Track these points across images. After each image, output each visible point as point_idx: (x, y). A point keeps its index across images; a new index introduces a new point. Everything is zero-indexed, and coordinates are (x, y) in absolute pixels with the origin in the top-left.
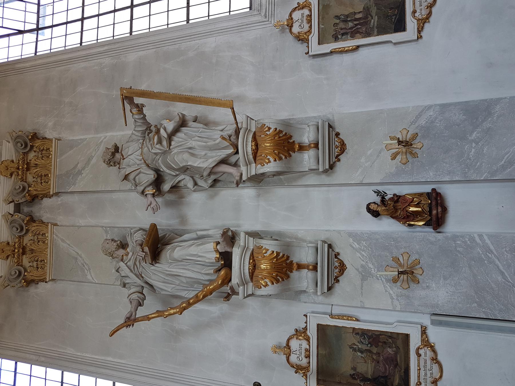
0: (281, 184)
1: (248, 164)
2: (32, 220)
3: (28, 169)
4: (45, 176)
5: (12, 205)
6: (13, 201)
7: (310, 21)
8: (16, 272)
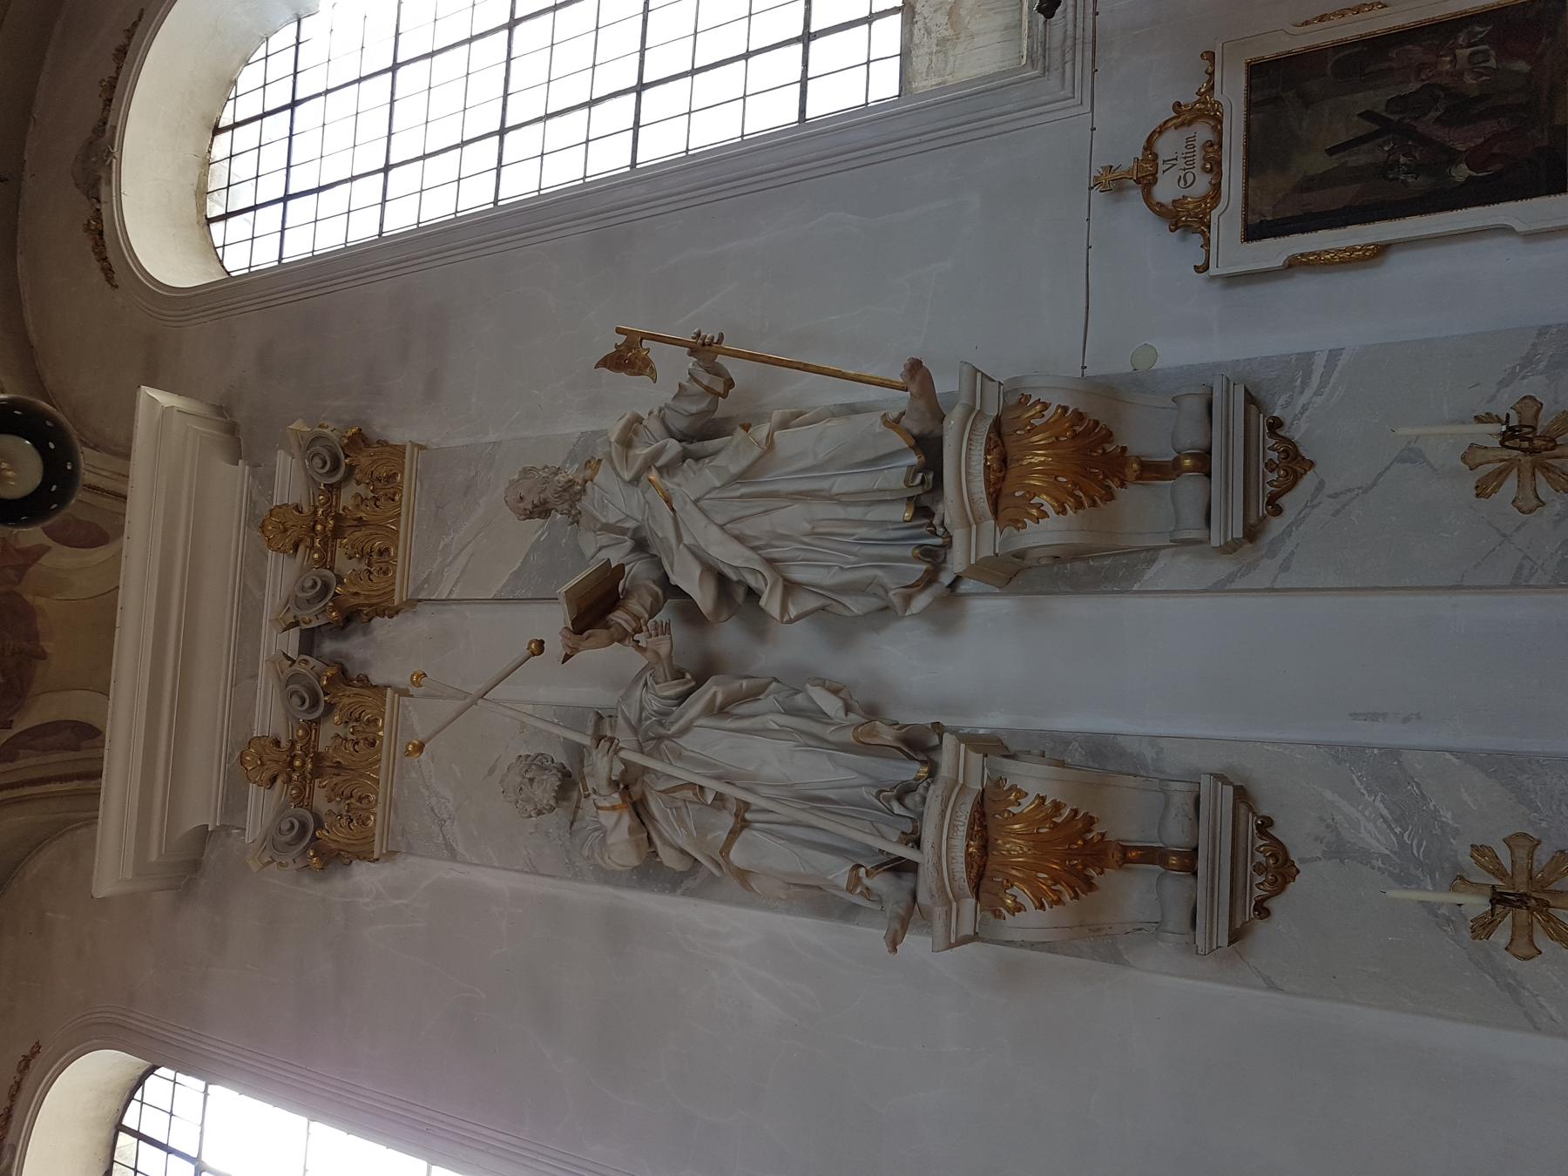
0: (1077, 587)
1: (971, 522)
2: (343, 675)
3: (337, 533)
4: (381, 553)
5: (294, 633)
6: (296, 624)
7: (1214, 166)
8: (315, 583)
